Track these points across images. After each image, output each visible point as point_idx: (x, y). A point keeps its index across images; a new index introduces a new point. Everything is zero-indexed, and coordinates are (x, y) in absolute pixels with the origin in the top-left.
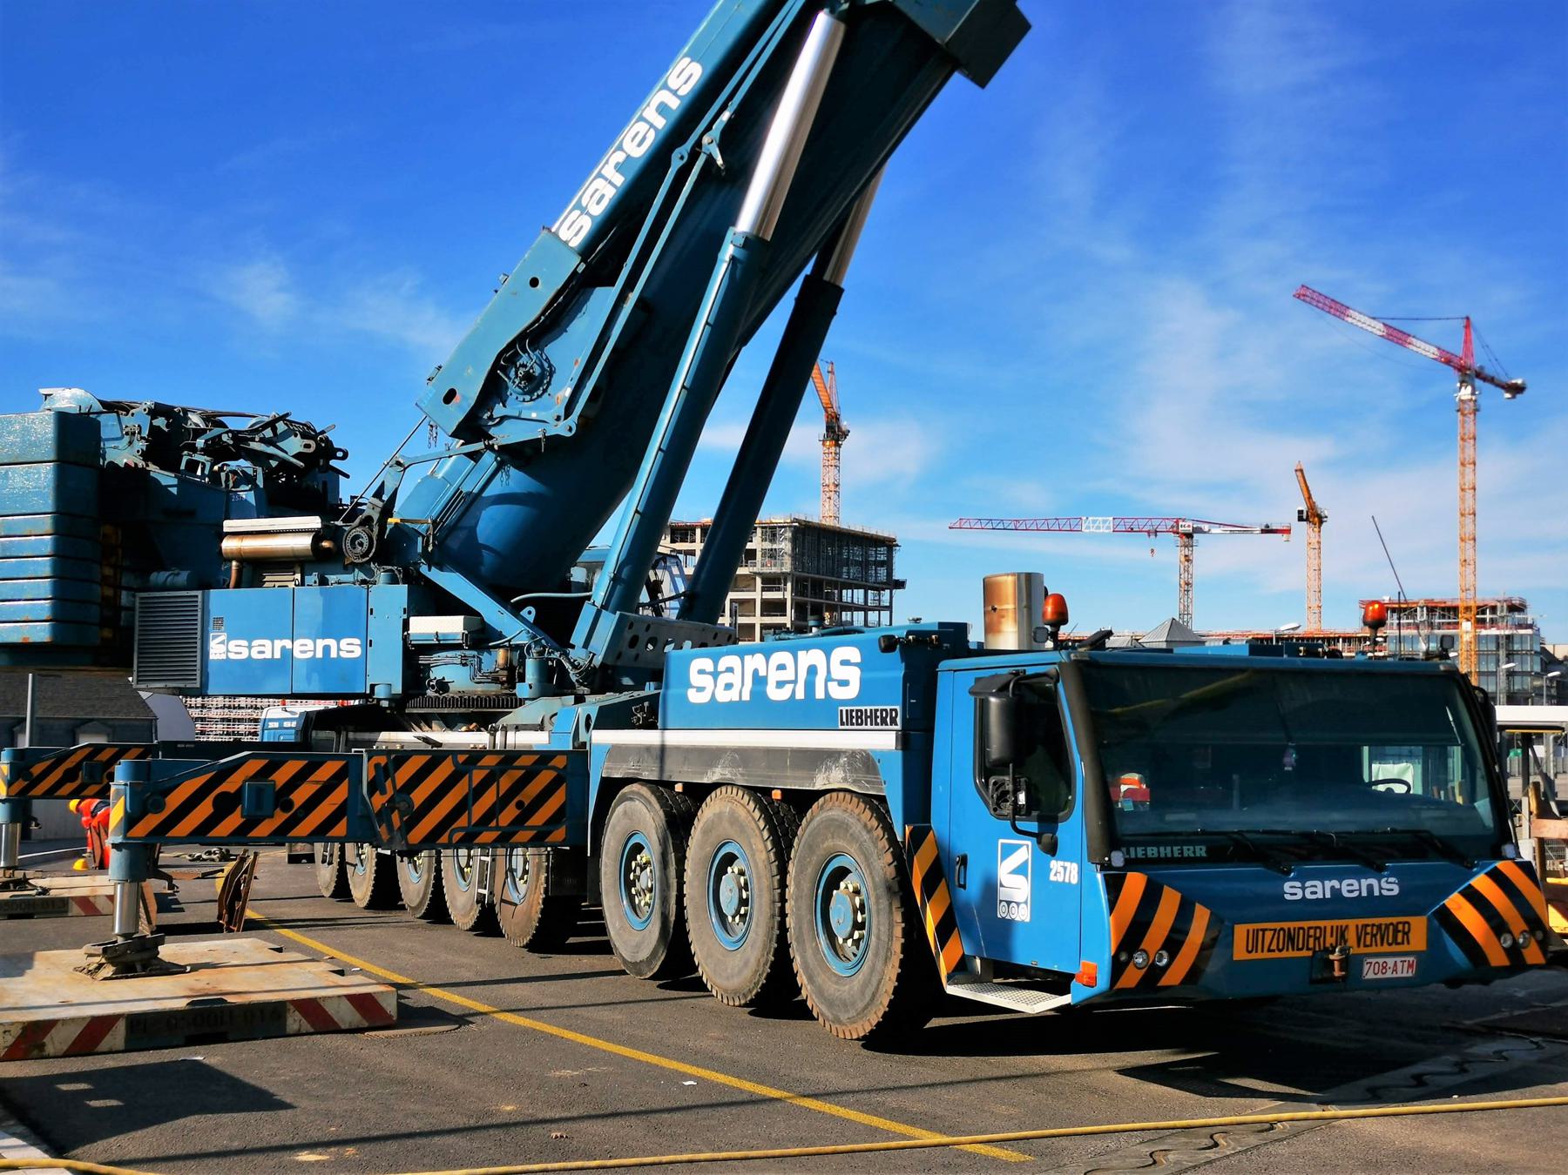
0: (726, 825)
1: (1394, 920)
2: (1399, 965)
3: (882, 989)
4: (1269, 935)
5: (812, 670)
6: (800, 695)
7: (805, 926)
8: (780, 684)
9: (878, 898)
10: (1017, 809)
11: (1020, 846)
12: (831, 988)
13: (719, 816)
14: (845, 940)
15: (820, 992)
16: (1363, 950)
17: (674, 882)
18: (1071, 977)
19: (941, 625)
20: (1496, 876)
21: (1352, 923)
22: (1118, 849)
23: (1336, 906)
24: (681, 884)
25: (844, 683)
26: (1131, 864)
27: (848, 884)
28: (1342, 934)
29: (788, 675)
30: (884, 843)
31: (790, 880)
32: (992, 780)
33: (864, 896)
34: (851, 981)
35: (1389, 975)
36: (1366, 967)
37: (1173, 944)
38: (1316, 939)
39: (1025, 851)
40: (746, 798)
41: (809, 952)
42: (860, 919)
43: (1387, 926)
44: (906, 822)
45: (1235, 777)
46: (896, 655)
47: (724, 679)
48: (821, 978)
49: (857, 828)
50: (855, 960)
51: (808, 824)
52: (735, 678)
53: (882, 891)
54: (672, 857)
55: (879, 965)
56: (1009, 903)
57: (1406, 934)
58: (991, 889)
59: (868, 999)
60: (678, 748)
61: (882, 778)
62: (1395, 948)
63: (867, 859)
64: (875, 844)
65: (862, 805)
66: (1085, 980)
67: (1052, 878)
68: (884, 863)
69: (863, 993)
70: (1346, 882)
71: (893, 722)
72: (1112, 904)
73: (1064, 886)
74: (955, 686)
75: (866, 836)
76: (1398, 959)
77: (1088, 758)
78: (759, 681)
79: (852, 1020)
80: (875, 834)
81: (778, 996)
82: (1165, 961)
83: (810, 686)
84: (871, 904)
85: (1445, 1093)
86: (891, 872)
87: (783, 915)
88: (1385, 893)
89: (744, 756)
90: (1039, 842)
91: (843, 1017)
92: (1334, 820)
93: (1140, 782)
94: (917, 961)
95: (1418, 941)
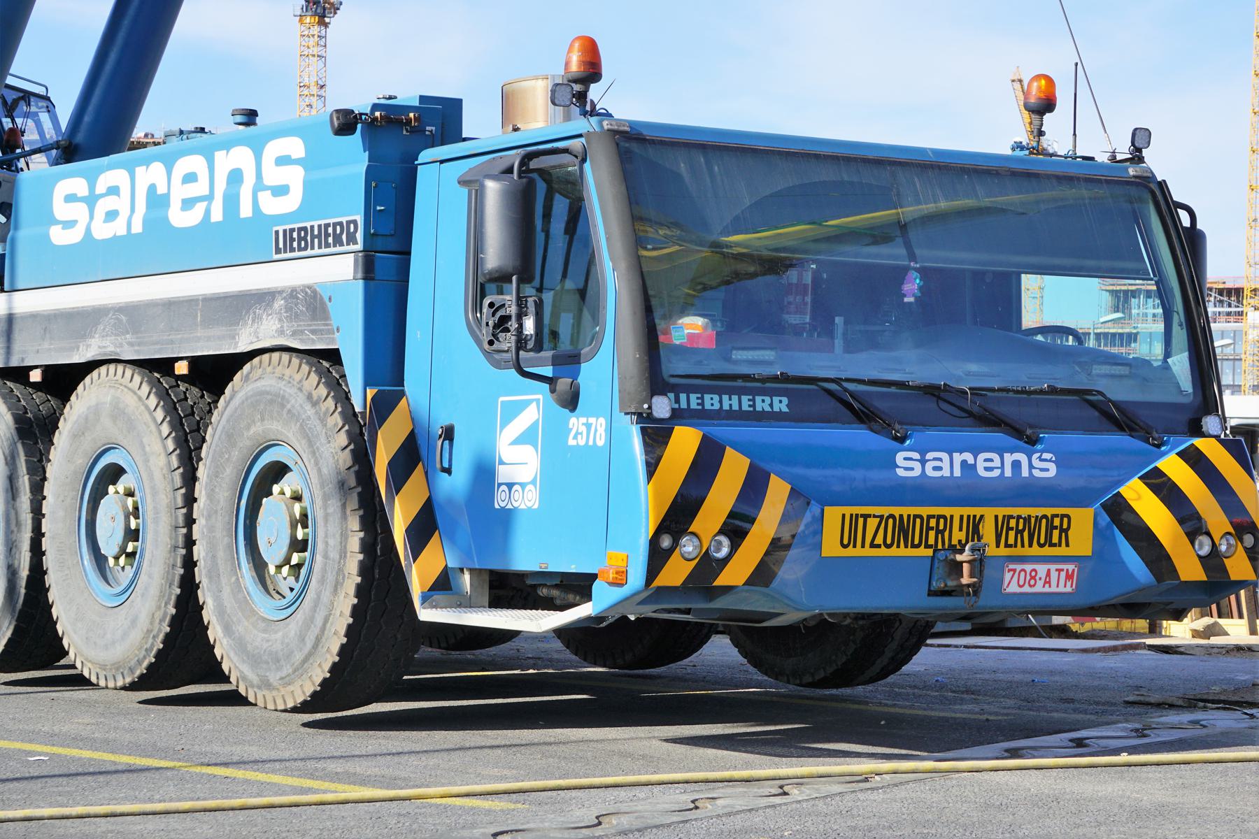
0: (106, 421)
1: (1049, 511)
2: (1054, 575)
3: (331, 629)
4: (872, 523)
5: (235, 177)
6: (217, 215)
7: (221, 554)
8: (188, 204)
9: (326, 498)
10: (521, 342)
11: (526, 404)
12: (257, 639)
13: (96, 410)
14: (279, 567)
15: (241, 646)
16: (1002, 551)
17: (27, 518)
18: (593, 577)
19: (423, 99)
20: (1195, 459)
21: (989, 513)
22: (663, 393)
23: (969, 492)
24: (38, 514)
25: (281, 191)
26: (679, 416)
27: (287, 485)
28: (974, 527)
29: (201, 188)
30: (337, 419)
31: (200, 490)
32: (487, 302)
33: (306, 502)
34: (283, 633)
35: (1039, 588)
36: (1008, 576)
37: (736, 529)
38: (938, 532)
39: (535, 404)
40: (137, 379)
41: (226, 592)
42: (300, 535)
43: (1038, 520)
44: (367, 383)
45: (839, 320)
46: (355, 140)
47: (103, 206)
48: (243, 626)
49: (297, 401)
50: (290, 596)
51: (228, 403)
52: (120, 203)
53: (331, 487)
54: (24, 482)
55: (326, 596)
56: (510, 486)
57: (1064, 531)
58: (485, 474)
59: (309, 645)
60: (34, 316)
61: (334, 323)
62: (1048, 551)
63: (311, 444)
64: (323, 421)
65: (305, 368)
66: (611, 576)
67: (571, 442)
68: (334, 449)
69: (302, 639)
70: (982, 456)
71: (352, 239)
72: (651, 468)
73: (589, 450)
74: (438, 185)
75: (310, 411)
76: (1053, 567)
77: (623, 265)
78: (157, 201)
79: (287, 681)
80: (323, 406)
81: (184, 663)
82: (725, 551)
83: (231, 201)
84: (318, 515)
85: (1116, 752)
86: (346, 458)
87: (190, 543)
88: (1036, 473)
89: (133, 315)
90: (553, 391)
91: (274, 678)
92: (966, 371)
93: (705, 328)
94: (381, 580)
95: (1082, 539)
